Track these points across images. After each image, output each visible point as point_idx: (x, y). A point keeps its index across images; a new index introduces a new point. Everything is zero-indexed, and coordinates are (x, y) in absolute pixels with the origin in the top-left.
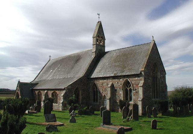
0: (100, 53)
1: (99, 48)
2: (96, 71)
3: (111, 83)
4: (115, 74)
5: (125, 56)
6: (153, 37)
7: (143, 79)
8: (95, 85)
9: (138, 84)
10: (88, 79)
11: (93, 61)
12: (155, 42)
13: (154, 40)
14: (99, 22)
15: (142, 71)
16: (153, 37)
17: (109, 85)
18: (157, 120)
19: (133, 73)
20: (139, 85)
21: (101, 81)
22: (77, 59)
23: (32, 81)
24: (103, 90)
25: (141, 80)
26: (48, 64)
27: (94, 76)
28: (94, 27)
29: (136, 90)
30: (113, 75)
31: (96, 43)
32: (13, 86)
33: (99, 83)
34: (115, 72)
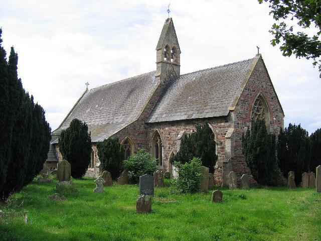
0: (169, 75)
1: (169, 68)
2: (160, 109)
3: (182, 132)
4: (188, 116)
5: (213, 80)
6: (258, 48)
7: (233, 125)
8: (157, 135)
9: (225, 134)
10: (148, 124)
11: (156, 92)
12: (261, 56)
13: (259, 54)
14: (167, 20)
15: (232, 111)
16: (258, 48)
17: (180, 136)
18: (237, 190)
19: (217, 115)
20: (226, 136)
21: (167, 128)
22: (133, 86)
23: (60, 124)
24: (169, 144)
25: (229, 126)
26: (85, 96)
27: (152, 120)
28: (155, 34)
29: (221, 143)
30: (184, 117)
31: (163, 59)
32: (19, 77)
33: (164, 132)
34: (191, 112)
